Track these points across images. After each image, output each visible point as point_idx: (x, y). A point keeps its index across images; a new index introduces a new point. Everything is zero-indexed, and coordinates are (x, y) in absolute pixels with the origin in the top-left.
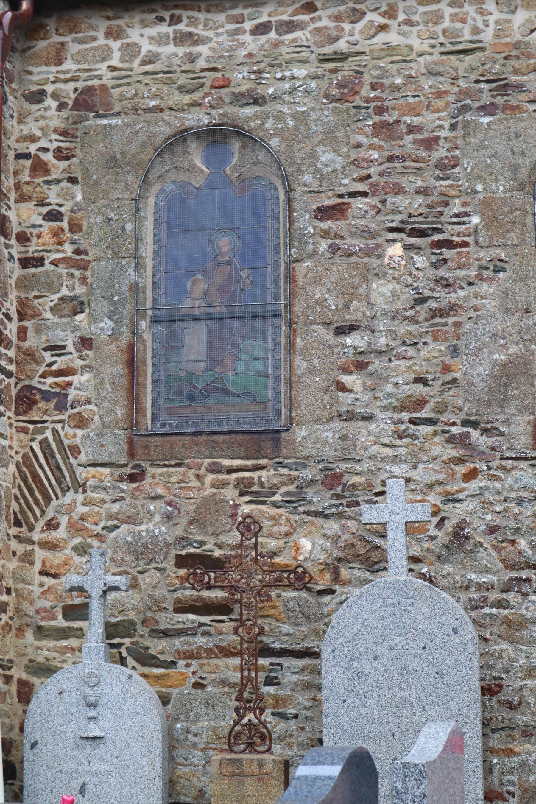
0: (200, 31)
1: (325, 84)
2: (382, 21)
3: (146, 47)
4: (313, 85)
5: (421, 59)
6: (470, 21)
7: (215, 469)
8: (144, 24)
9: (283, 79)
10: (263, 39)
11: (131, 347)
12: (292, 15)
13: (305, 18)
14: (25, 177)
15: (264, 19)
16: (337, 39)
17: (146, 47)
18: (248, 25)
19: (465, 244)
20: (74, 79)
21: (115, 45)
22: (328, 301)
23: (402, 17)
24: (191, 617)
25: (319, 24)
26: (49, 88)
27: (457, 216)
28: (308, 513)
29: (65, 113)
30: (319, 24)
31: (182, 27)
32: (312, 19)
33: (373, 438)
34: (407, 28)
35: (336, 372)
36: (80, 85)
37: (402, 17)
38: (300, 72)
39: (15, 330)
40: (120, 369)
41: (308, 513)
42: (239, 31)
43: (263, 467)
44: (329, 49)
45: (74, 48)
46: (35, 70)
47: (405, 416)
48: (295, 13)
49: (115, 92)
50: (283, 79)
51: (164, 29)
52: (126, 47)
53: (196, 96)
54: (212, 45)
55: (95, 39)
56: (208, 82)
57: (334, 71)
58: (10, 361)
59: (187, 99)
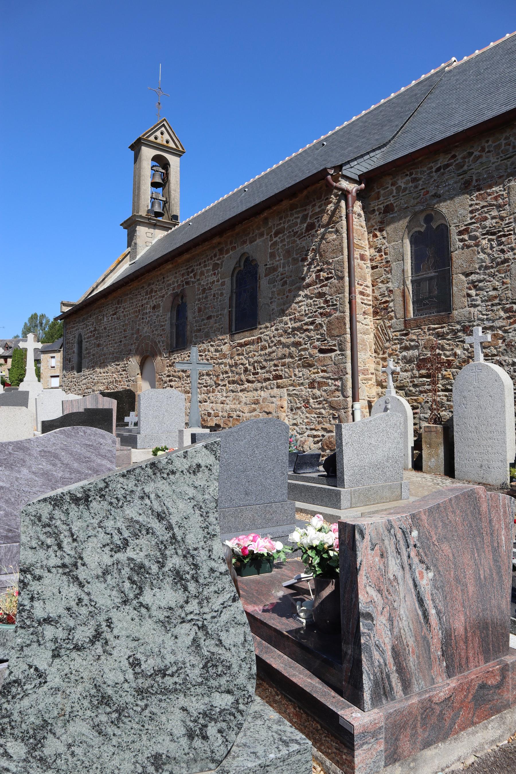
0: (419, 176)
1: (459, 184)
2: (479, 154)
3: (403, 186)
4: (455, 185)
5: (494, 166)
6: (512, 144)
7: (429, 329)
8: (402, 178)
9: (446, 186)
10: (439, 173)
11: (404, 290)
12: (449, 160)
13: (452, 161)
14: (371, 240)
15: (439, 165)
16: (464, 165)
17: (403, 186)
18: (434, 170)
19: (510, 234)
20: (383, 203)
21: (394, 188)
22: (111, 677)
23: (487, 150)
24: (424, 379)
25: (457, 162)
26: (376, 208)
27: (508, 224)
28: (459, 341)
29: (381, 215)
30: (457, 162)
31: (413, 176)
32: (455, 161)
33: (149, 732)
34: (489, 154)
35: (466, 290)
36: (385, 204)
37: (487, 150)
38: (451, 182)
39: (371, 290)
40: (401, 299)
41: (459, 341)
42: (432, 172)
43: (444, 327)
44: (461, 171)
45: (382, 192)
46: (371, 203)
47: (490, 303)
48: (449, 160)
49: (395, 205)
50: (446, 186)
51: (408, 178)
52: (397, 188)
53: (419, 200)
54: (423, 180)
55: (388, 187)
56: (422, 194)
57: (462, 179)
58: (370, 300)
59: (416, 201)
